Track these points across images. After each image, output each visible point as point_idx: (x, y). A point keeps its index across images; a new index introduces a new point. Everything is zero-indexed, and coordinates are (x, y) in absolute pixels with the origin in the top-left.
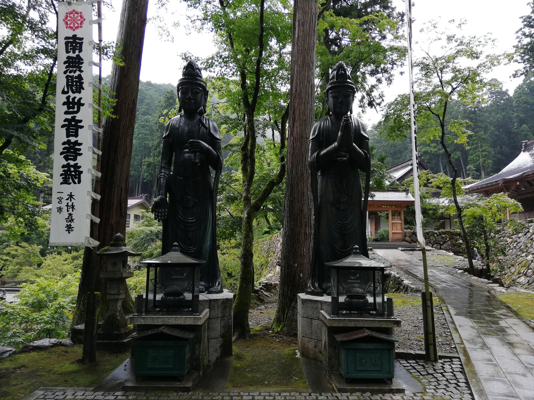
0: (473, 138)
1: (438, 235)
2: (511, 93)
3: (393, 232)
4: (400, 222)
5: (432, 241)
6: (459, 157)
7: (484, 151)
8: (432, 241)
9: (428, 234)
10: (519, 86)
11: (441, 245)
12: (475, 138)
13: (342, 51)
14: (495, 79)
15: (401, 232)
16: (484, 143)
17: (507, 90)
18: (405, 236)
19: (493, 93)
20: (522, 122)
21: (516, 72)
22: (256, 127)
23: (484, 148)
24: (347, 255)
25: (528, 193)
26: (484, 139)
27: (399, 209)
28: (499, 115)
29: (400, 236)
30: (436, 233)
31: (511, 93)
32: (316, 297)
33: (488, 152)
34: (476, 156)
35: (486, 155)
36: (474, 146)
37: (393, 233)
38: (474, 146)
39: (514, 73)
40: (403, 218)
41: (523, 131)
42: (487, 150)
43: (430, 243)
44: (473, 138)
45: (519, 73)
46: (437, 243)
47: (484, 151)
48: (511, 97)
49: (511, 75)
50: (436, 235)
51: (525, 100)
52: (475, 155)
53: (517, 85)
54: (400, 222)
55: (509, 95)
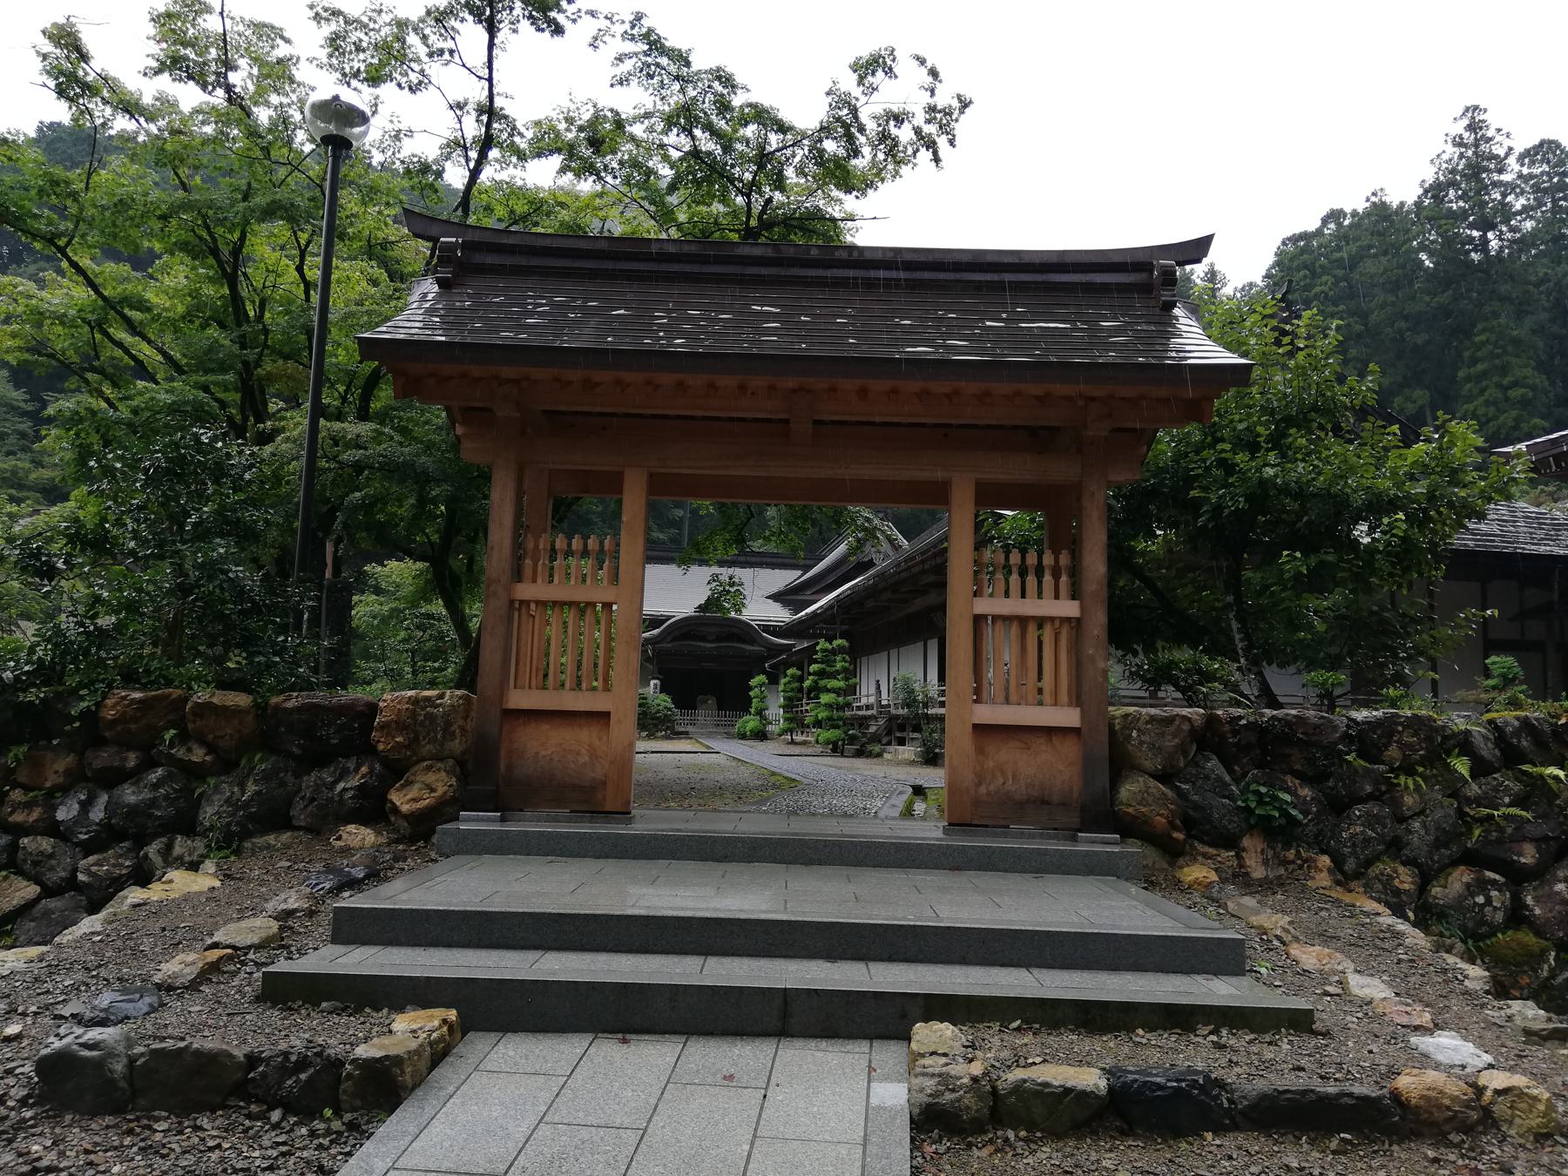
0: (1477, 339)
1: (1481, 769)
3: (987, 714)
4: (1069, 609)
5: (1418, 834)
6: (1422, 408)
7: (1515, 384)
8: (1418, 834)
9: (1370, 752)
11: (1517, 877)
12: (1483, 338)
13: (1212, 446)
14: (1551, 142)
15: (1069, 717)
16: (1518, 356)
18: (1119, 763)
19: (1545, 191)
22: (665, 216)
26: (1516, 342)
27: (1059, 470)
29: (1057, 769)
30: (1464, 744)
32: (713, 962)
33: (1533, 388)
34: (1487, 403)
35: (1524, 403)
36: (1480, 367)
37: (979, 729)
38: (1480, 367)
40: (1096, 564)
43: (1395, 847)
44: (1477, 339)
46: (1470, 859)
47: (1515, 384)
50: (1462, 766)
54: (1069, 609)
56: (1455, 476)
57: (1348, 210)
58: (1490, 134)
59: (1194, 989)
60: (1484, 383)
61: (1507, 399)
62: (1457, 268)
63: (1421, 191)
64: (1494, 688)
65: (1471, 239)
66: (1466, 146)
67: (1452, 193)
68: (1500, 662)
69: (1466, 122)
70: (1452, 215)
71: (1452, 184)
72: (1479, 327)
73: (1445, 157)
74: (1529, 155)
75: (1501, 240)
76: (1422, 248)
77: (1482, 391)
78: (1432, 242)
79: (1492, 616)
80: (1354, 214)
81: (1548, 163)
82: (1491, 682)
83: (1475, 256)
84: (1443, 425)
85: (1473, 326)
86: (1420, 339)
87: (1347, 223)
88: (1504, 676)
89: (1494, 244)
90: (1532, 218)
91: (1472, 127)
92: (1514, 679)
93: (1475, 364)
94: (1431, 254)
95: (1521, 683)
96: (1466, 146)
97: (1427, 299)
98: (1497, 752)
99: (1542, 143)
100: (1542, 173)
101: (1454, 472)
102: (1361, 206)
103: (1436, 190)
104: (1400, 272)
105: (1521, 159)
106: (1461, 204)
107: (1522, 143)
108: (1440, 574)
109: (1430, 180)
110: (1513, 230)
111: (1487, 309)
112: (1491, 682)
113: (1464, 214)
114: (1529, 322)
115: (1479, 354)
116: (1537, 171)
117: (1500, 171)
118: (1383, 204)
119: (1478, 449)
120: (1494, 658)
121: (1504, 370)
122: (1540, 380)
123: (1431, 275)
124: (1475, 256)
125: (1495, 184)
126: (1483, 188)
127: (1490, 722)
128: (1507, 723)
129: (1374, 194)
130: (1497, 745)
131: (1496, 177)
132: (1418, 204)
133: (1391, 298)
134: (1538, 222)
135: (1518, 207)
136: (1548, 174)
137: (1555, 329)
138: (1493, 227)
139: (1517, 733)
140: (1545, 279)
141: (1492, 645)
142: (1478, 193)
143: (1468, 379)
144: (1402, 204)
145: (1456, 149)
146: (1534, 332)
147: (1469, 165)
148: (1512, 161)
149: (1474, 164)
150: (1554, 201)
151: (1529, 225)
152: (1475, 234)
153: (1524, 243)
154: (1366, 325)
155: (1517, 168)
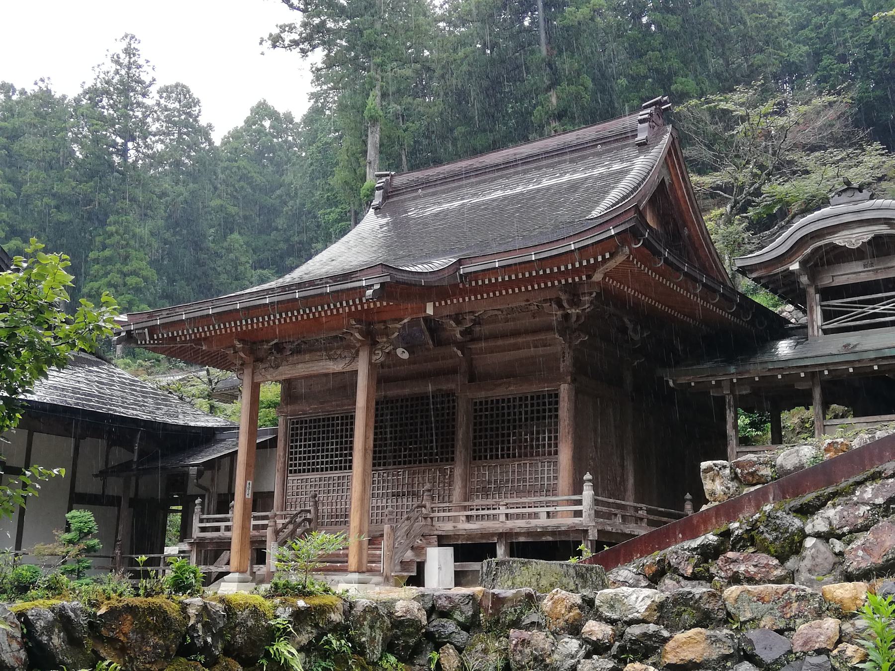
2: (217, 138)
7: (135, 273)
10: (236, 130)
14: (183, 86)
17: (210, 126)
19: (175, 124)
20: (228, 226)
21: (283, 28)
23: (134, 265)
24: (595, 488)
25: (423, 376)
28: (180, 188)
31: (217, 138)
33: (146, 279)
35: (137, 290)
36: (107, 253)
38: (107, 253)
39: (276, 31)
41: (229, 250)
42: (144, 273)
44: (108, 228)
45: (288, 37)
47: (135, 273)
48: (217, 148)
49: (266, 37)
51: (245, 172)
52: (105, 280)
53: (231, 129)
55: (211, 143)
56: (40, 314)
57: (18, 87)
58: (141, 62)
59: (522, 151)
60: (109, 267)
61: (125, 285)
62: (99, 168)
63: (81, 91)
64: (70, 542)
65: (114, 144)
66: (120, 65)
67: (105, 101)
68: (81, 516)
69: (124, 45)
70: (102, 118)
71: (107, 93)
72: (112, 218)
73: (104, 68)
74: (166, 91)
75: (138, 151)
76: (75, 140)
77: (106, 274)
78: (85, 137)
79: (58, 476)
80: (23, 92)
81: (180, 102)
82: (68, 536)
83: (116, 159)
84: (34, 254)
85: (107, 216)
86: (64, 217)
87: (15, 98)
88: (80, 530)
89: (132, 153)
90: (162, 142)
91: (129, 52)
92: (89, 532)
93: (103, 250)
94: (83, 146)
95: (94, 537)
96: (120, 65)
97: (74, 184)
98: (23, 655)
99: (177, 85)
100: (174, 109)
101: (39, 310)
102: (31, 89)
103: (94, 94)
104: (54, 154)
105: (160, 92)
106: (111, 112)
107: (165, 79)
108: (14, 424)
109: (89, 84)
110: (147, 146)
111: (119, 205)
112: (68, 536)
113: (111, 122)
114: (150, 224)
115: (107, 241)
116: (171, 106)
117: (144, 95)
118: (49, 91)
119: (67, 288)
120: (74, 513)
121: (126, 259)
122: (150, 273)
123: (79, 164)
124: (116, 159)
125: (139, 104)
126: (128, 105)
127: (21, 615)
128: (39, 616)
129: (42, 80)
130: (24, 645)
131: (140, 99)
132: (77, 100)
133: (43, 175)
134: (167, 147)
135: (153, 128)
136: (179, 111)
137: (167, 235)
138: (133, 139)
139: (48, 630)
140: (164, 194)
141: (77, 499)
142: (125, 107)
143: (96, 261)
144: (64, 97)
145: (114, 65)
146: (152, 234)
147: (121, 82)
148: (153, 90)
149: (126, 86)
150: (180, 134)
151: (159, 147)
152: (119, 140)
153: (157, 159)
154: (19, 194)
155: (157, 97)
